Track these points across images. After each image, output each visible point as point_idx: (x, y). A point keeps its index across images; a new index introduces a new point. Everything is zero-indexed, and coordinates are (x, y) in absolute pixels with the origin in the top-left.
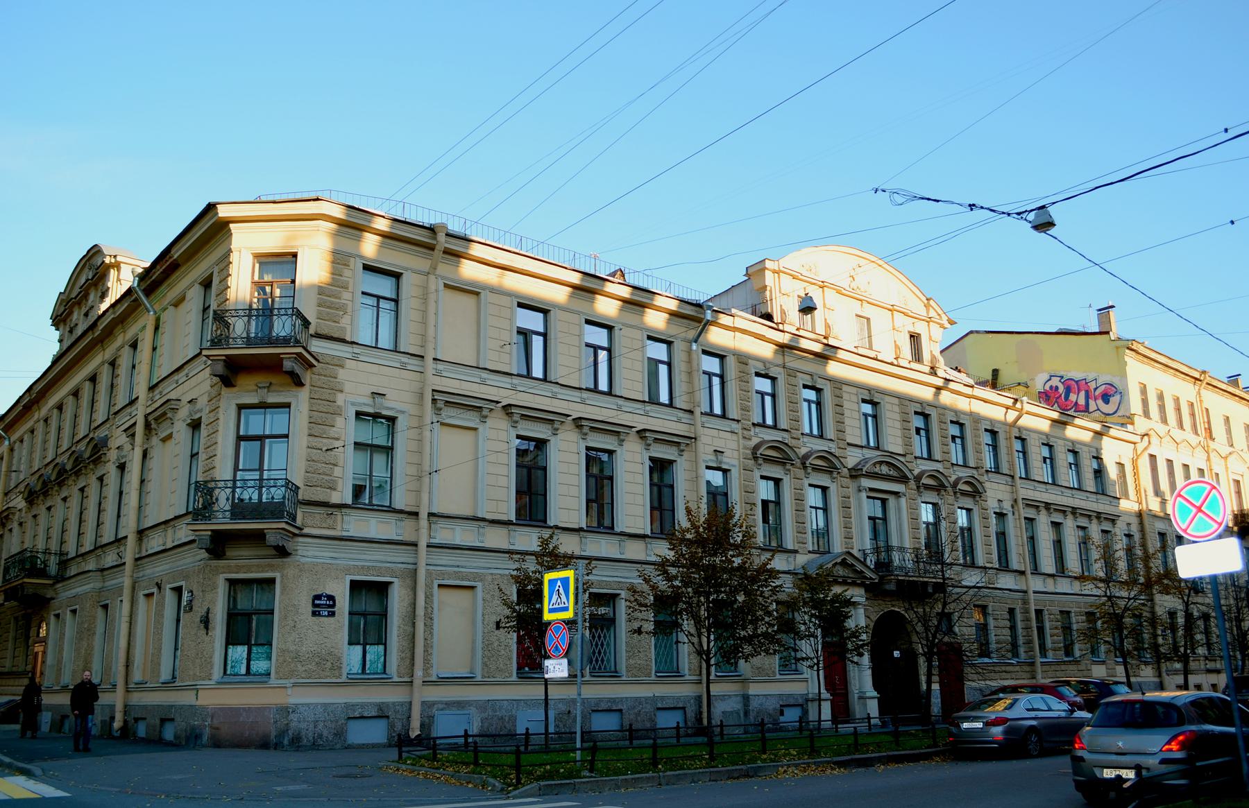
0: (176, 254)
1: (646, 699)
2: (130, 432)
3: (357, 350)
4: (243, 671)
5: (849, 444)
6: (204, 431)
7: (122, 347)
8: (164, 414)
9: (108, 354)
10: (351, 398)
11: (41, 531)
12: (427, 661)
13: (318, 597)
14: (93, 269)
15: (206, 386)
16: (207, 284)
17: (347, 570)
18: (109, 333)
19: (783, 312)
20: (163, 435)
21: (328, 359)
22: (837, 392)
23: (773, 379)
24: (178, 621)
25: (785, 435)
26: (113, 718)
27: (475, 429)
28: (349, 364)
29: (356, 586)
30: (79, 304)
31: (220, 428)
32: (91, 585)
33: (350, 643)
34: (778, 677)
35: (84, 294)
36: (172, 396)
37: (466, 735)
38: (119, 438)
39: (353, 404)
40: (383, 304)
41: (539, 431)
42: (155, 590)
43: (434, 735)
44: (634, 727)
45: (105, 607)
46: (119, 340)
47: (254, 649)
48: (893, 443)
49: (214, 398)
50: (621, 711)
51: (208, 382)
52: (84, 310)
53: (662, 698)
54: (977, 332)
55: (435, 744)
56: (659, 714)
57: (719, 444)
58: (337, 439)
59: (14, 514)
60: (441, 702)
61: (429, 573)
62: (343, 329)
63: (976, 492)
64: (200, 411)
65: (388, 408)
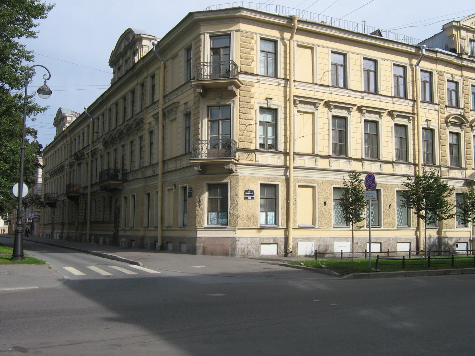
1: (393, 238)
2: (156, 117)
3: (259, 78)
4: (215, 223)
6: (192, 118)
7: (147, 77)
8: (173, 109)
9: (140, 80)
10: (257, 101)
11: (112, 159)
12: (294, 220)
13: (247, 191)
14: (129, 41)
15: (192, 97)
16: (188, 50)
17: (259, 179)
18: (141, 71)
19: (462, 48)
20: (172, 118)
21: (247, 83)
23: (457, 83)
25: (462, 111)
26: (156, 241)
27: (313, 113)
28: (256, 85)
29: (263, 186)
30: (122, 57)
31: (201, 116)
32: (141, 184)
35: (125, 52)
36: (175, 100)
37: (342, 253)
38: (149, 119)
40: (269, 55)
41: (343, 113)
42: (173, 187)
46: (145, 75)
49: (197, 103)
52: (125, 59)
53: (400, 238)
56: (398, 244)
59: (98, 152)
60: (300, 238)
61: (294, 180)
64: (190, 108)
65: (274, 105)
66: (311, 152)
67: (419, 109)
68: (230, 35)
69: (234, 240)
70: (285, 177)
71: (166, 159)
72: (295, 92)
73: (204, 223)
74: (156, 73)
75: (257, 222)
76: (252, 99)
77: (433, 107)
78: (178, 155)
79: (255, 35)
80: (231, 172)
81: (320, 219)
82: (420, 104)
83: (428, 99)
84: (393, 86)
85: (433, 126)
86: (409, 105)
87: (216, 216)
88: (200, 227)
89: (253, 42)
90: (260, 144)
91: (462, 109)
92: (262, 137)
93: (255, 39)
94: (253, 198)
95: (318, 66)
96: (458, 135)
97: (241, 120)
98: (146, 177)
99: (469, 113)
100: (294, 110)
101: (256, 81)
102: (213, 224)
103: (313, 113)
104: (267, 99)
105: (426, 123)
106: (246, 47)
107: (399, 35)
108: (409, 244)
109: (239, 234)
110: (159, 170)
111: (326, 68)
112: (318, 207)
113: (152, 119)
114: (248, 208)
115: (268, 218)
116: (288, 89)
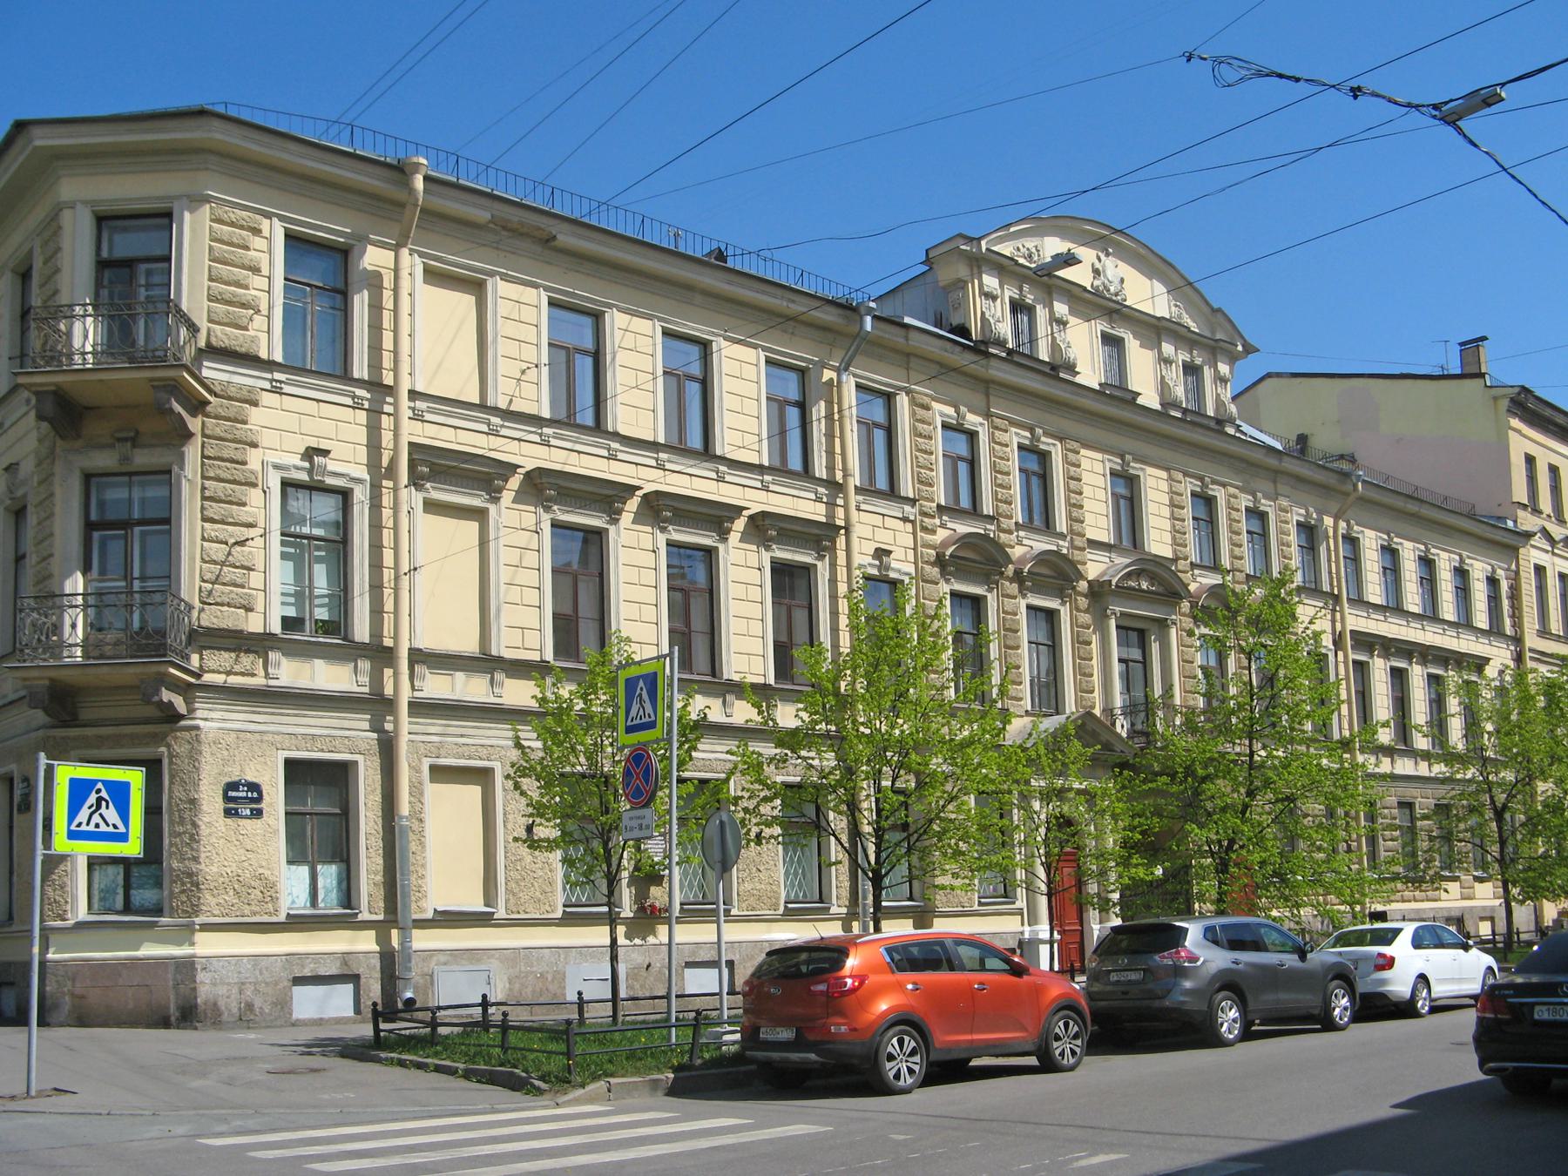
5: (1094, 544)
6: (32, 519)
10: (274, 458)
13: (233, 786)
15: (31, 442)
21: (232, 391)
22: (1071, 456)
24: (11, 828)
28: (267, 399)
29: (294, 769)
31: (57, 510)
33: (290, 862)
34: (976, 907)
39: (277, 467)
43: (433, 1003)
44: (586, 997)
48: (1158, 543)
49: (47, 459)
51: (34, 434)
54: (1279, 375)
55: (434, 1018)
57: (884, 539)
62: (254, 340)
67: (854, 513)
68: (168, 215)
69: (187, 967)
70: (375, 735)
72: (414, 432)
73: (75, 909)
75: (274, 900)
77: (893, 509)
80: (172, 717)
82: (854, 498)
83: (882, 483)
84: (765, 435)
85: (899, 571)
86: (818, 500)
88: (59, 923)
90: (285, 620)
91: (990, 519)
92: (292, 590)
93: (266, 233)
94: (258, 814)
95: (501, 348)
96: (977, 602)
97: (207, 525)
99: (1010, 532)
100: (412, 499)
101: (267, 385)
103: (479, 515)
104: (311, 453)
105: (296, 460)
106: (229, 260)
107: (784, 268)
116: (386, 421)
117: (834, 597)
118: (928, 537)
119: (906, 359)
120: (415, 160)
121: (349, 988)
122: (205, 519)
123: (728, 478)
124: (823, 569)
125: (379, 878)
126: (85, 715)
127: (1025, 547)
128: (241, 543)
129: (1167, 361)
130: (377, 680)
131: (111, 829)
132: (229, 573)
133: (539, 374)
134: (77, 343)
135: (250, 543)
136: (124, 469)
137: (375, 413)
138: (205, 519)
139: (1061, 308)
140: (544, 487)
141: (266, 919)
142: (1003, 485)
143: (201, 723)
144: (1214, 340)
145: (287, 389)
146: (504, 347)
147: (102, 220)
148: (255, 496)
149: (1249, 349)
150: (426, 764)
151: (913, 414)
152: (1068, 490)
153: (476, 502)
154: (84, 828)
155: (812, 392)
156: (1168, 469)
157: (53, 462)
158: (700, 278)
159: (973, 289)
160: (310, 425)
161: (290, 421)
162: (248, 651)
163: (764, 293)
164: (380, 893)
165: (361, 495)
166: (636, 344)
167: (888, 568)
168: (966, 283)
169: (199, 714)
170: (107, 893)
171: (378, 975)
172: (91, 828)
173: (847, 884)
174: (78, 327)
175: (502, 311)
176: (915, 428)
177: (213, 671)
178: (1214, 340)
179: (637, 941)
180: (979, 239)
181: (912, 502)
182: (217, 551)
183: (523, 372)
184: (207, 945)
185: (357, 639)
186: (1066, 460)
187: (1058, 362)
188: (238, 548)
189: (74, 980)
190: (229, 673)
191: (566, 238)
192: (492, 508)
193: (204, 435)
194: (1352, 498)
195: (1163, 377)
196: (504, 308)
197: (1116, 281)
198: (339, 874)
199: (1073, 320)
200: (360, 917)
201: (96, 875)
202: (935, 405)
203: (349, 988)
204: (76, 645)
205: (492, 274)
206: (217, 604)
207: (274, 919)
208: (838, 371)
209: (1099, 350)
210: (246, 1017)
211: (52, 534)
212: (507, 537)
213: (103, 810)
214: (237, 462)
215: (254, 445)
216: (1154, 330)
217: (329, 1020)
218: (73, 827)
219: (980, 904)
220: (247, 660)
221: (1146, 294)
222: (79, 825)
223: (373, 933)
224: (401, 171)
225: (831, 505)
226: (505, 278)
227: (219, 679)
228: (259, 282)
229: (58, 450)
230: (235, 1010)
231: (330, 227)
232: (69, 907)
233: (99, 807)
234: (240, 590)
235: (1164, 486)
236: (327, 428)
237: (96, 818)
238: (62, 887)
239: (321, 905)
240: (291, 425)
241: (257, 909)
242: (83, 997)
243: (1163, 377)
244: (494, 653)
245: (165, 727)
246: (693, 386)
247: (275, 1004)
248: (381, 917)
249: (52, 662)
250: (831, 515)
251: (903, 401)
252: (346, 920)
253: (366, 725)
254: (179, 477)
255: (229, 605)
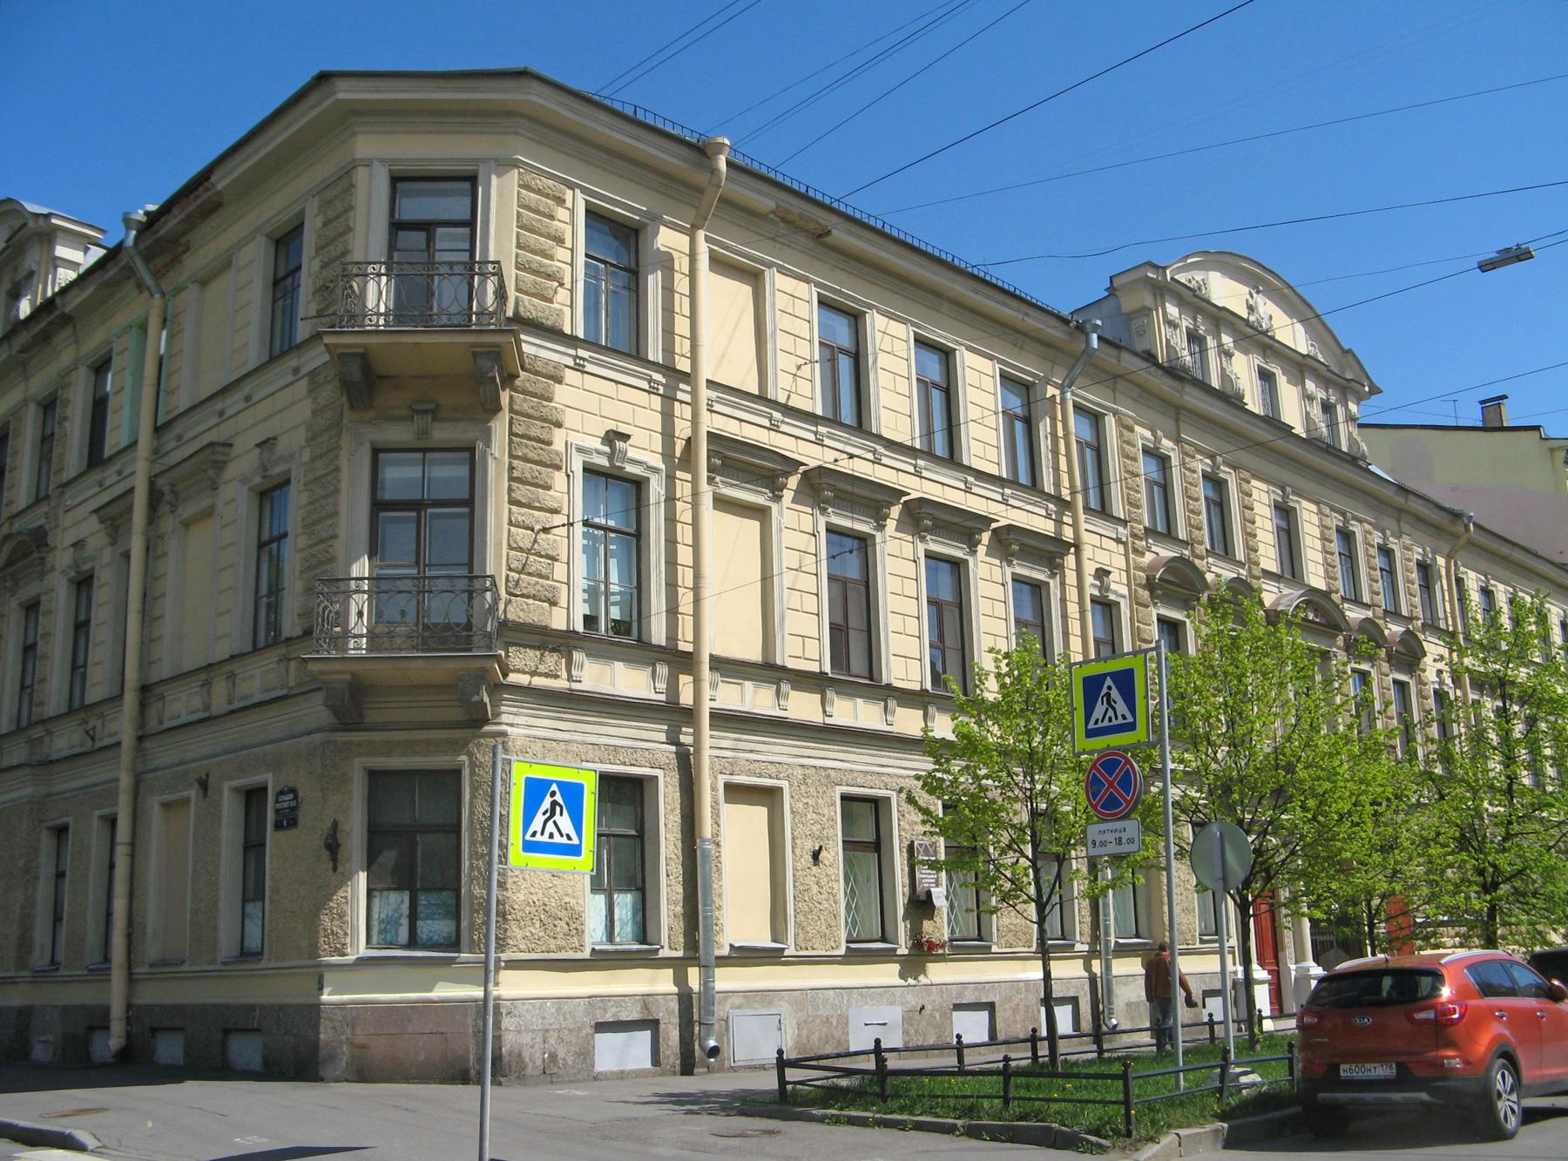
0: (221, 182)
2: (114, 517)
5: (1267, 574)
7: (73, 368)
10: (577, 439)
15: (304, 411)
21: (539, 366)
22: (1244, 485)
28: (570, 376)
29: (606, 780)
31: (344, 485)
37: (878, 1050)
38: (77, 525)
39: (580, 450)
42: (193, 793)
44: (965, 1040)
45: (61, 832)
47: (423, 899)
49: (325, 441)
50: (990, 1007)
57: (1103, 559)
58: (555, 511)
62: (560, 313)
63: (1408, 656)
66: (754, 654)
68: (472, 179)
70: (673, 748)
71: (154, 678)
72: (709, 423)
73: (355, 942)
74: (117, 348)
76: (557, 431)
78: (219, 658)
79: (569, 193)
81: (801, 917)
85: (1116, 593)
86: (1048, 516)
87: (405, 908)
88: (336, 959)
89: (562, 214)
90: (585, 616)
91: (1185, 543)
93: (569, 204)
97: (514, 508)
98: (51, 762)
102: (391, 945)
103: (760, 513)
104: (614, 437)
105: (596, 444)
108: (985, 1014)
109: (512, 986)
110: (123, 725)
111: (804, 349)
112: (795, 869)
113: (90, 528)
114: (544, 870)
115: (616, 917)
117: (1065, 617)
118: (1139, 559)
119: (1113, 380)
120: (720, 140)
121: (646, 1035)
122: (512, 502)
123: (975, 490)
124: (1054, 585)
125: (679, 909)
126: (372, 717)
127: (1217, 572)
128: (546, 530)
129: (1309, 398)
130: (673, 688)
131: (564, 840)
132: (536, 563)
133: (813, 370)
134: (371, 304)
135: (555, 531)
136: (421, 444)
137: (669, 399)
138: (512, 502)
139: (1227, 340)
140: (823, 487)
141: (571, 955)
142: (1191, 514)
143: (509, 729)
144: (1342, 377)
145: (589, 368)
146: (783, 341)
147: (397, 180)
148: (559, 479)
149: (1375, 390)
150: (722, 779)
151: (1121, 435)
152: (1244, 519)
153: (760, 500)
154: (538, 838)
155: (1038, 408)
156: (1317, 503)
157: (339, 435)
158: (950, 284)
159: (1158, 316)
160: (610, 408)
161: (591, 402)
162: (553, 650)
163: (1004, 304)
164: (679, 926)
165: (656, 489)
166: (891, 343)
167: (1108, 589)
168: (1150, 310)
169: (504, 718)
170: (390, 923)
171: (676, 1020)
172: (545, 838)
173: (1088, 919)
174: (372, 287)
175: (780, 304)
176: (1123, 450)
177: (518, 671)
178: (1342, 377)
179: (911, 981)
180: (1164, 268)
181: (1124, 523)
182: (523, 537)
183: (799, 368)
184: (512, 986)
185: (655, 641)
186: (1239, 487)
187: (1228, 391)
188: (543, 535)
189: (353, 1028)
190: (533, 673)
191: (841, 235)
192: (774, 507)
193: (511, 410)
194: (1462, 541)
195: (1307, 413)
196: (782, 301)
197: (1266, 318)
198: (634, 904)
199: (1237, 353)
200: (662, 954)
201: (376, 902)
202: (1137, 428)
203: (646, 1035)
204: (362, 636)
205: (770, 265)
206: (522, 596)
207: (579, 956)
208: (1061, 387)
209: (1257, 383)
210: (550, 1072)
211: (336, 514)
212: (789, 538)
213: (557, 817)
214: (543, 442)
215: (559, 425)
216: (1300, 367)
217: (630, 1072)
218: (528, 837)
219: (1202, 942)
220: (551, 660)
221: (1292, 335)
222: (534, 834)
223: (670, 972)
224: (702, 152)
225: (1059, 522)
226: (782, 271)
227: (523, 679)
228: (562, 254)
229: (345, 420)
230: (539, 1062)
231: (627, 203)
232: (348, 940)
233: (553, 814)
234: (545, 582)
235: (1315, 519)
236: (624, 412)
237: (550, 827)
238: (341, 916)
239: (618, 940)
240: (592, 407)
241: (563, 943)
242: (364, 1047)
243: (1307, 413)
244: (779, 662)
245: (467, 733)
246: (941, 393)
247: (578, 1054)
248: (680, 954)
249: (334, 654)
250: (1059, 531)
251: (1110, 422)
252: (646, 959)
253: (663, 737)
254: (485, 453)
255: (534, 597)
